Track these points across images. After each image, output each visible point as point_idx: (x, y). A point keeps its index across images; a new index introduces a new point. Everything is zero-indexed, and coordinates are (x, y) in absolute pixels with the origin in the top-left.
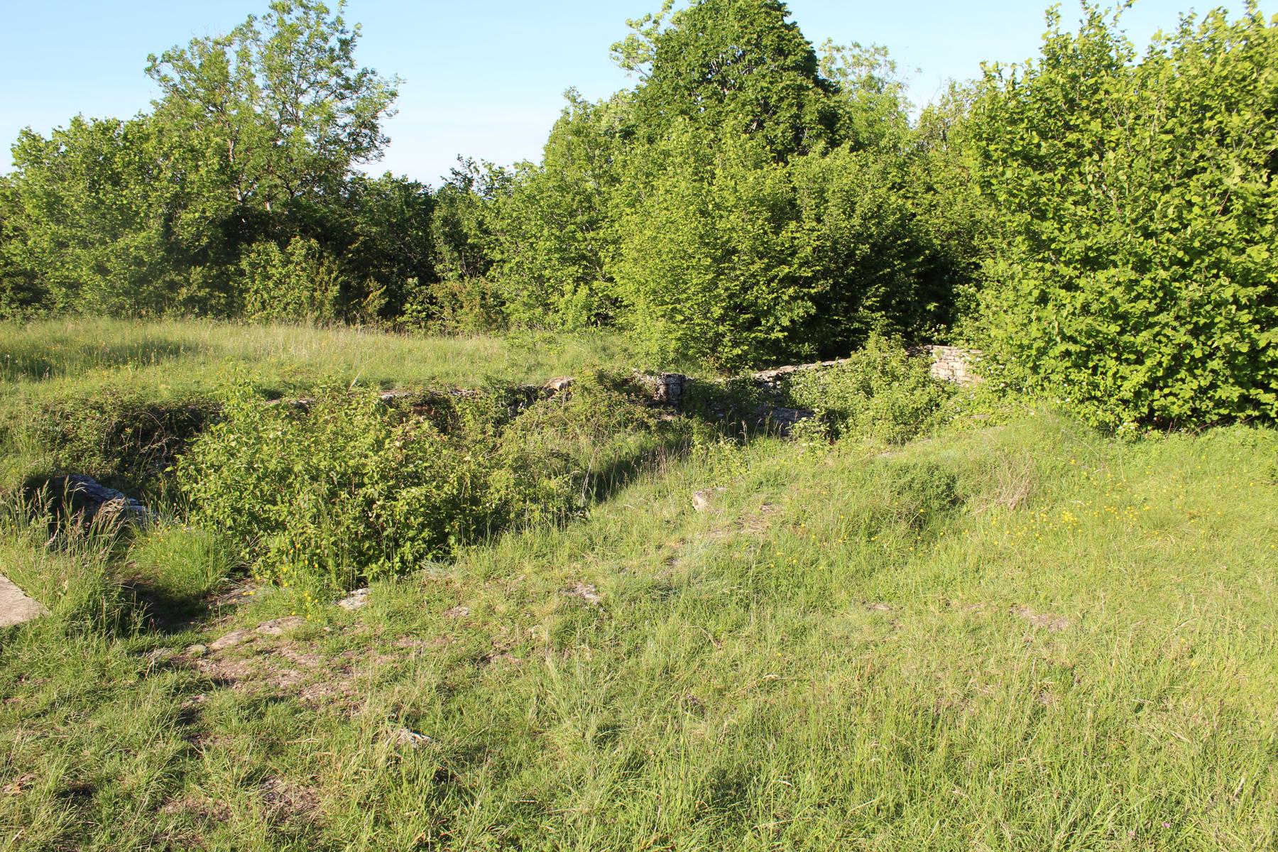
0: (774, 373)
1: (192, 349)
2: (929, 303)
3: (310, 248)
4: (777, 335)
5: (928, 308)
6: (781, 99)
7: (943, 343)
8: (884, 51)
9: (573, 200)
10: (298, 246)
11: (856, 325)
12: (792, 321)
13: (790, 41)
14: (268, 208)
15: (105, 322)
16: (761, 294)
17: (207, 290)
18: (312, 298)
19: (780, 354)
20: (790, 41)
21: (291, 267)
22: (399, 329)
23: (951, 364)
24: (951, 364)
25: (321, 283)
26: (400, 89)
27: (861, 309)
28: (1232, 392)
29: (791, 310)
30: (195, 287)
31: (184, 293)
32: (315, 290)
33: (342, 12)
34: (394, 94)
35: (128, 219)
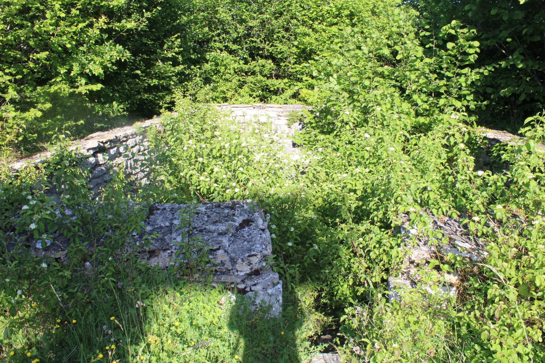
11: (155, 82)
12: (105, 68)
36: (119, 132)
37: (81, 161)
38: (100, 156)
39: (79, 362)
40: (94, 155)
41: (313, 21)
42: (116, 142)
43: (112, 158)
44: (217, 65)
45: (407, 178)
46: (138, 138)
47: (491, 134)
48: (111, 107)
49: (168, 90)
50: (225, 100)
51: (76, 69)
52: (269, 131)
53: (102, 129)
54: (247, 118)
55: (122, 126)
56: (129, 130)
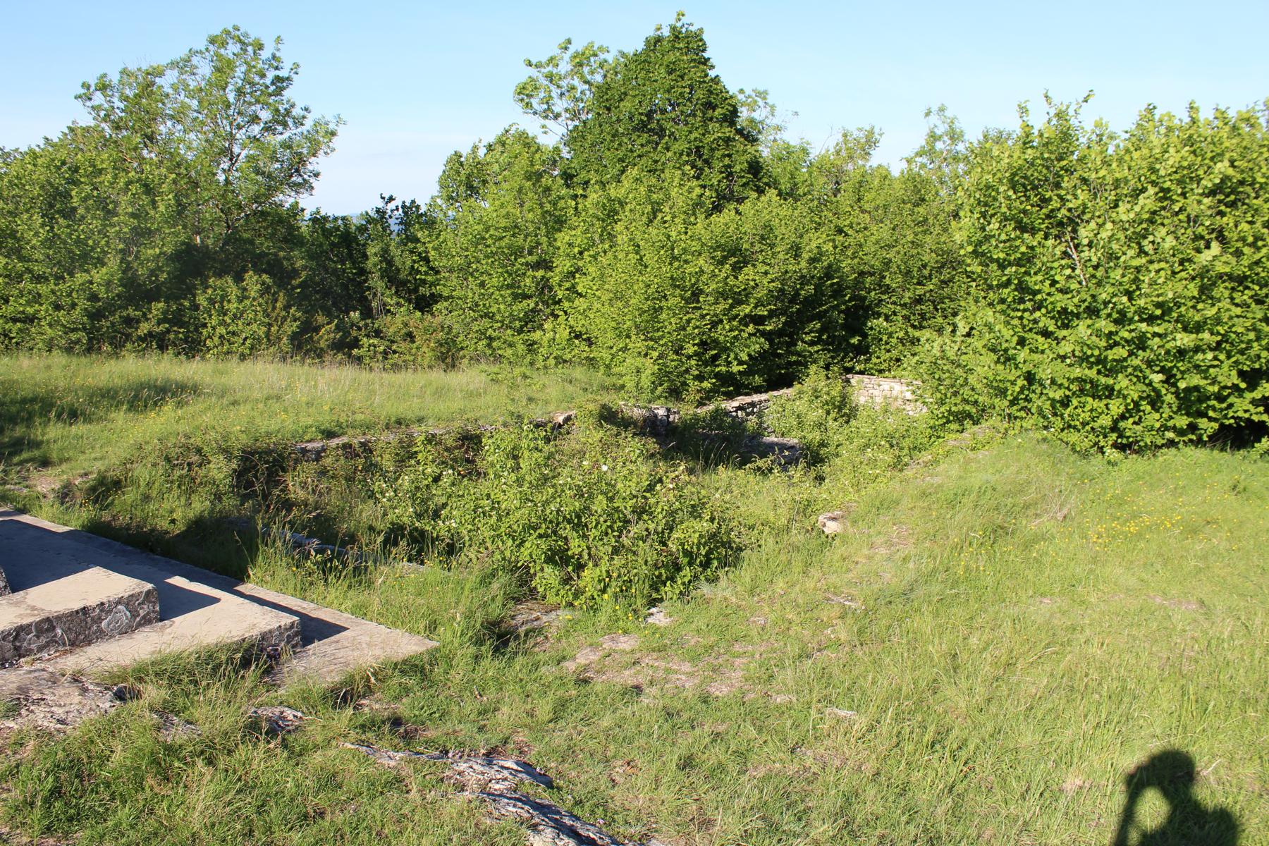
0: (736, 404)
1: (195, 390)
2: (853, 336)
3: (263, 283)
4: (735, 368)
5: (852, 341)
6: (712, 150)
7: (861, 373)
8: (763, 95)
9: (525, 241)
10: (252, 281)
11: (794, 358)
12: (749, 355)
13: (717, 95)
14: (199, 241)
15: (58, 359)
16: (722, 333)
17: (167, 326)
18: (268, 335)
19: (732, 385)
20: (717, 95)
21: (247, 302)
22: (396, 367)
23: (870, 391)
24: (870, 391)
25: (276, 318)
26: (341, 130)
27: (800, 343)
28: (1182, 421)
29: (749, 347)
30: (154, 321)
31: (144, 328)
32: (270, 325)
33: (278, 50)
34: (333, 134)
35: (86, 258)
36: (756, 398)
37: (727, 413)
38: (740, 413)
39: (10, 344)
41: (273, 295)
42: (753, 405)
43: (748, 414)
45: (442, 776)
47: (711, 407)
48: (754, 378)
50: (880, 371)
51: (732, 356)
53: (747, 394)
54: (895, 393)
56: (764, 397)
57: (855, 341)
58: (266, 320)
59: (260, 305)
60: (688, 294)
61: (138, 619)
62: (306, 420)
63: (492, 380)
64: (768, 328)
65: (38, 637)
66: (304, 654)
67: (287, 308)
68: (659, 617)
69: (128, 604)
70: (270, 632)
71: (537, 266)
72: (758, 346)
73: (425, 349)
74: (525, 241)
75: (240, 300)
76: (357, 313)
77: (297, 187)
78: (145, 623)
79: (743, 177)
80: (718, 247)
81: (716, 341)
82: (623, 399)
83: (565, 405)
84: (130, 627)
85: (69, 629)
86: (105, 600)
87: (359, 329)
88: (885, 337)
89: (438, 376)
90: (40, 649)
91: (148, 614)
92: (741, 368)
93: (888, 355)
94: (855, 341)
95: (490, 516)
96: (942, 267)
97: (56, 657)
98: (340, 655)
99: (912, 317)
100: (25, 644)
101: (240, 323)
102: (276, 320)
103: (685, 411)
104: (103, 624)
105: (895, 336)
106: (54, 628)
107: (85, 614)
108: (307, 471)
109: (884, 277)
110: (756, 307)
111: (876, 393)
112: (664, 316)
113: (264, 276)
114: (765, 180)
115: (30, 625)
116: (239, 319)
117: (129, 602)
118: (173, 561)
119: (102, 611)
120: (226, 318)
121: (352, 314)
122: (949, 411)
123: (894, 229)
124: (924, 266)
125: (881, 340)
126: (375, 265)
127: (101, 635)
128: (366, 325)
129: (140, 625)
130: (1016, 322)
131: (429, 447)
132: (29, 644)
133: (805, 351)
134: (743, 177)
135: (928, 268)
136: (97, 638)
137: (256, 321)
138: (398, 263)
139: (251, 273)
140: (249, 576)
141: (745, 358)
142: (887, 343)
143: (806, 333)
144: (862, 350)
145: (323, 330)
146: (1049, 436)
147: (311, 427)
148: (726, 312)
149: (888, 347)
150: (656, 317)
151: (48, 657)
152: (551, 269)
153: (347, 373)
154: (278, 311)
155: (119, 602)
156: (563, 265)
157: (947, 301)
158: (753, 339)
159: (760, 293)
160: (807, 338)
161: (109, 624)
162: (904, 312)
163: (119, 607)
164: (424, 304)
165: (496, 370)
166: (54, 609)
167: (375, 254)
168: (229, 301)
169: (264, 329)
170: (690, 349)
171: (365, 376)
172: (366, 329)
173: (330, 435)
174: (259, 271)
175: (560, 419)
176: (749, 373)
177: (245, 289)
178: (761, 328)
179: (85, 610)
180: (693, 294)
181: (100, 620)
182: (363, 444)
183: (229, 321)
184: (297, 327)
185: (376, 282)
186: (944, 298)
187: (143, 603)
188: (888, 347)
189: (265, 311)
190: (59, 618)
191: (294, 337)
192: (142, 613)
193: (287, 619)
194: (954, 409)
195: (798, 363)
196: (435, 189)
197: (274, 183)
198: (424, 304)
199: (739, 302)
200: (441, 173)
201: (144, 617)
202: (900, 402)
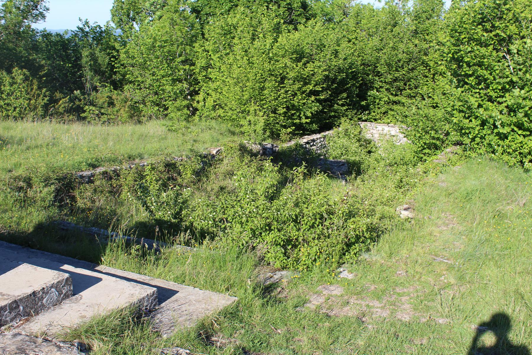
3: (25, 74)
4: (304, 121)
7: (366, 121)
9: (177, 48)
10: (18, 74)
11: (333, 114)
12: (312, 113)
18: (29, 104)
21: (15, 86)
24: (371, 131)
27: (336, 105)
29: (311, 108)
32: (30, 99)
36: (314, 136)
37: (301, 146)
40: (305, 145)
42: (313, 141)
43: (311, 146)
44: (374, 98)
46: (322, 139)
49: (339, 118)
50: (375, 120)
52: (465, 12)
53: (309, 135)
54: (385, 132)
55: (316, 134)
56: (318, 136)
57: (363, 103)
58: (28, 96)
59: (24, 88)
60: (279, 79)
61: (62, 296)
62: (77, 159)
63: (169, 130)
64: (322, 97)
65: (10, 313)
66: (162, 310)
67: (40, 88)
68: (346, 274)
69: (57, 287)
70: (143, 298)
71: (184, 62)
72: (316, 108)
73: (122, 111)
74: (177, 48)
75: (11, 85)
76: (78, 91)
77: (36, 18)
78: (65, 298)
79: (298, 11)
80: (294, 52)
81: (293, 106)
82: (246, 140)
83: (215, 144)
84: (58, 301)
85: (27, 306)
86: (44, 286)
87: (80, 100)
88: (377, 101)
89: (130, 128)
90: (12, 320)
91: (67, 292)
92: (308, 121)
93: (379, 111)
94: (363, 103)
95: (242, 217)
96: (410, 61)
97: (22, 324)
98: (184, 309)
99: (391, 89)
100: (4, 318)
101: (12, 98)
102: (33, 96)
103: (283, 146)
104: (44, 301)
105: (383, 100)
106: (18, 306)
107: (34, 296)
108: (88, 191)
109: (377, 67)
110: (315, 86)
111: (374, 132)
112: (266, 92)
113: (24, 70)
114: (310, 12)
115: (6, 306)
116: (11, 96)
117: (56, 286)
118: (46, 253)
119: (43, 293)
120: (3, 95)
121: (75, 92)
122: (425, 144)
123: (381, 40)
124: (399, 61)
125: (375, 102)
126: (87, 62)
127: (43, 308)
128: (85, 98)
129: (63, 299)
130: (477, 95)
131: (153, 172)
132: (6, 318)
133: (338, 109)
134: (298, 11)
135: (402, 62)
136: (41, 310)
137: (21, 97)
138: (100, 61)
139: (16, 68)
140: (101, 261)
141: (309, 115)
142: (378, 104)
143: (339, 100)
144: (366, 108)
145: (61, 102)
146: (495, 158)
147: (82, 162)
148: (299, 89)
149: (379, 106)
150: (261, 93)
151: (17, 325)
152: (194, 64)
153: (77, 128)
154: (34, 91)
155: (52, 287)
156: (201, 63)
157: (412, 80)
158: (313, 104)
159: (319, 77)
160: (340, 103)
161: (47, 301)
162: (388, 86)
163: (53, 289)
164: (117, 85)
165: (171, 124)
166: (16, 295)
167: (87, 56)
168: (4, 85)
169: (27, 102)
170: (281, 111)
171: (91, 128)
172: (85, 100)
173: (94, 166)
174: (21, 68)
175: (214, 152)
176: (311, 123)
177: (13, 78)
178: (318, 97)
179: (34, 293)
180: (282, 79)
181: (43, 298)
182: (115, 171)
183: (5, 97)
184: (48, 100)
185: (88, 74)
186: (411, 78)
187: (64, 286)
188: (379, 106)
189: (26, 91)
190: (21, 300)
191: (46, 107)
192: (64, 292)
193: (67, 275)
194: (427, 142)
195: (335, 116)
196: (109, 17)
197: (26, 13)
198: (117, 85)
199: (306, 84)
200: (111, 8)
201: (65, 294)
202: (388, 136)
